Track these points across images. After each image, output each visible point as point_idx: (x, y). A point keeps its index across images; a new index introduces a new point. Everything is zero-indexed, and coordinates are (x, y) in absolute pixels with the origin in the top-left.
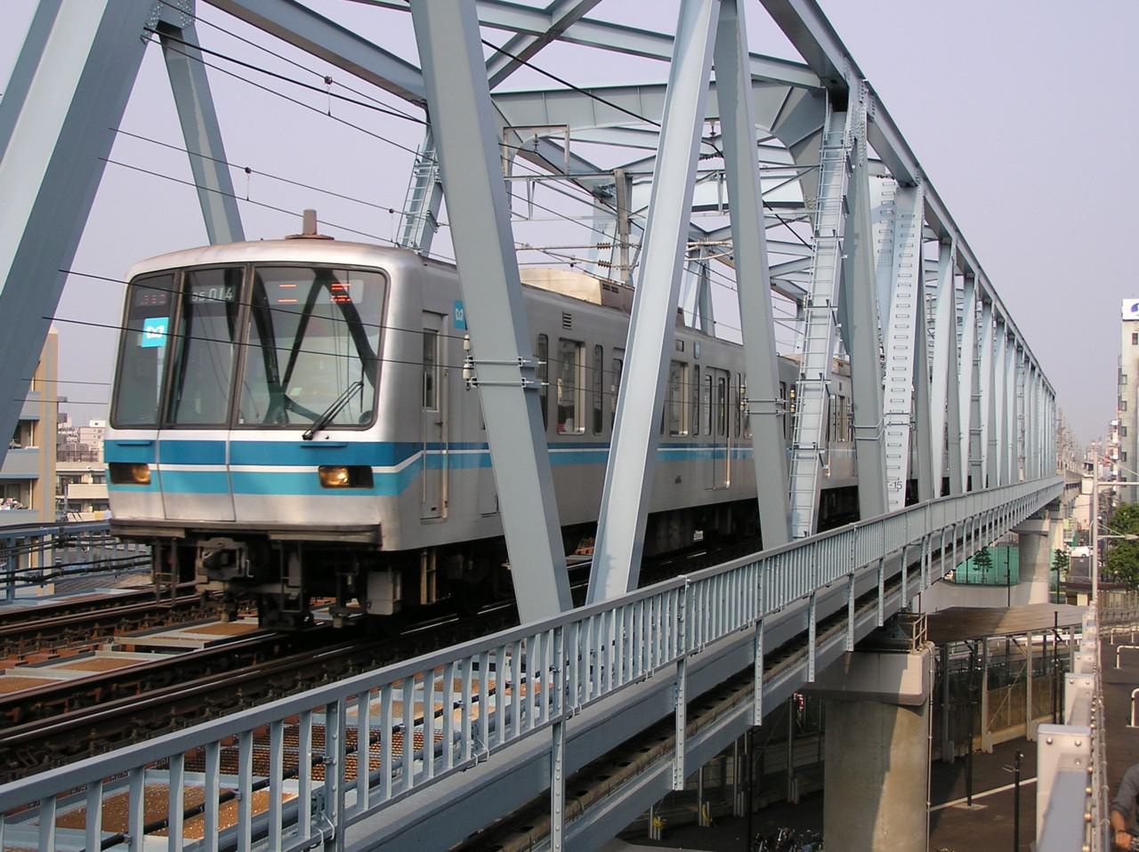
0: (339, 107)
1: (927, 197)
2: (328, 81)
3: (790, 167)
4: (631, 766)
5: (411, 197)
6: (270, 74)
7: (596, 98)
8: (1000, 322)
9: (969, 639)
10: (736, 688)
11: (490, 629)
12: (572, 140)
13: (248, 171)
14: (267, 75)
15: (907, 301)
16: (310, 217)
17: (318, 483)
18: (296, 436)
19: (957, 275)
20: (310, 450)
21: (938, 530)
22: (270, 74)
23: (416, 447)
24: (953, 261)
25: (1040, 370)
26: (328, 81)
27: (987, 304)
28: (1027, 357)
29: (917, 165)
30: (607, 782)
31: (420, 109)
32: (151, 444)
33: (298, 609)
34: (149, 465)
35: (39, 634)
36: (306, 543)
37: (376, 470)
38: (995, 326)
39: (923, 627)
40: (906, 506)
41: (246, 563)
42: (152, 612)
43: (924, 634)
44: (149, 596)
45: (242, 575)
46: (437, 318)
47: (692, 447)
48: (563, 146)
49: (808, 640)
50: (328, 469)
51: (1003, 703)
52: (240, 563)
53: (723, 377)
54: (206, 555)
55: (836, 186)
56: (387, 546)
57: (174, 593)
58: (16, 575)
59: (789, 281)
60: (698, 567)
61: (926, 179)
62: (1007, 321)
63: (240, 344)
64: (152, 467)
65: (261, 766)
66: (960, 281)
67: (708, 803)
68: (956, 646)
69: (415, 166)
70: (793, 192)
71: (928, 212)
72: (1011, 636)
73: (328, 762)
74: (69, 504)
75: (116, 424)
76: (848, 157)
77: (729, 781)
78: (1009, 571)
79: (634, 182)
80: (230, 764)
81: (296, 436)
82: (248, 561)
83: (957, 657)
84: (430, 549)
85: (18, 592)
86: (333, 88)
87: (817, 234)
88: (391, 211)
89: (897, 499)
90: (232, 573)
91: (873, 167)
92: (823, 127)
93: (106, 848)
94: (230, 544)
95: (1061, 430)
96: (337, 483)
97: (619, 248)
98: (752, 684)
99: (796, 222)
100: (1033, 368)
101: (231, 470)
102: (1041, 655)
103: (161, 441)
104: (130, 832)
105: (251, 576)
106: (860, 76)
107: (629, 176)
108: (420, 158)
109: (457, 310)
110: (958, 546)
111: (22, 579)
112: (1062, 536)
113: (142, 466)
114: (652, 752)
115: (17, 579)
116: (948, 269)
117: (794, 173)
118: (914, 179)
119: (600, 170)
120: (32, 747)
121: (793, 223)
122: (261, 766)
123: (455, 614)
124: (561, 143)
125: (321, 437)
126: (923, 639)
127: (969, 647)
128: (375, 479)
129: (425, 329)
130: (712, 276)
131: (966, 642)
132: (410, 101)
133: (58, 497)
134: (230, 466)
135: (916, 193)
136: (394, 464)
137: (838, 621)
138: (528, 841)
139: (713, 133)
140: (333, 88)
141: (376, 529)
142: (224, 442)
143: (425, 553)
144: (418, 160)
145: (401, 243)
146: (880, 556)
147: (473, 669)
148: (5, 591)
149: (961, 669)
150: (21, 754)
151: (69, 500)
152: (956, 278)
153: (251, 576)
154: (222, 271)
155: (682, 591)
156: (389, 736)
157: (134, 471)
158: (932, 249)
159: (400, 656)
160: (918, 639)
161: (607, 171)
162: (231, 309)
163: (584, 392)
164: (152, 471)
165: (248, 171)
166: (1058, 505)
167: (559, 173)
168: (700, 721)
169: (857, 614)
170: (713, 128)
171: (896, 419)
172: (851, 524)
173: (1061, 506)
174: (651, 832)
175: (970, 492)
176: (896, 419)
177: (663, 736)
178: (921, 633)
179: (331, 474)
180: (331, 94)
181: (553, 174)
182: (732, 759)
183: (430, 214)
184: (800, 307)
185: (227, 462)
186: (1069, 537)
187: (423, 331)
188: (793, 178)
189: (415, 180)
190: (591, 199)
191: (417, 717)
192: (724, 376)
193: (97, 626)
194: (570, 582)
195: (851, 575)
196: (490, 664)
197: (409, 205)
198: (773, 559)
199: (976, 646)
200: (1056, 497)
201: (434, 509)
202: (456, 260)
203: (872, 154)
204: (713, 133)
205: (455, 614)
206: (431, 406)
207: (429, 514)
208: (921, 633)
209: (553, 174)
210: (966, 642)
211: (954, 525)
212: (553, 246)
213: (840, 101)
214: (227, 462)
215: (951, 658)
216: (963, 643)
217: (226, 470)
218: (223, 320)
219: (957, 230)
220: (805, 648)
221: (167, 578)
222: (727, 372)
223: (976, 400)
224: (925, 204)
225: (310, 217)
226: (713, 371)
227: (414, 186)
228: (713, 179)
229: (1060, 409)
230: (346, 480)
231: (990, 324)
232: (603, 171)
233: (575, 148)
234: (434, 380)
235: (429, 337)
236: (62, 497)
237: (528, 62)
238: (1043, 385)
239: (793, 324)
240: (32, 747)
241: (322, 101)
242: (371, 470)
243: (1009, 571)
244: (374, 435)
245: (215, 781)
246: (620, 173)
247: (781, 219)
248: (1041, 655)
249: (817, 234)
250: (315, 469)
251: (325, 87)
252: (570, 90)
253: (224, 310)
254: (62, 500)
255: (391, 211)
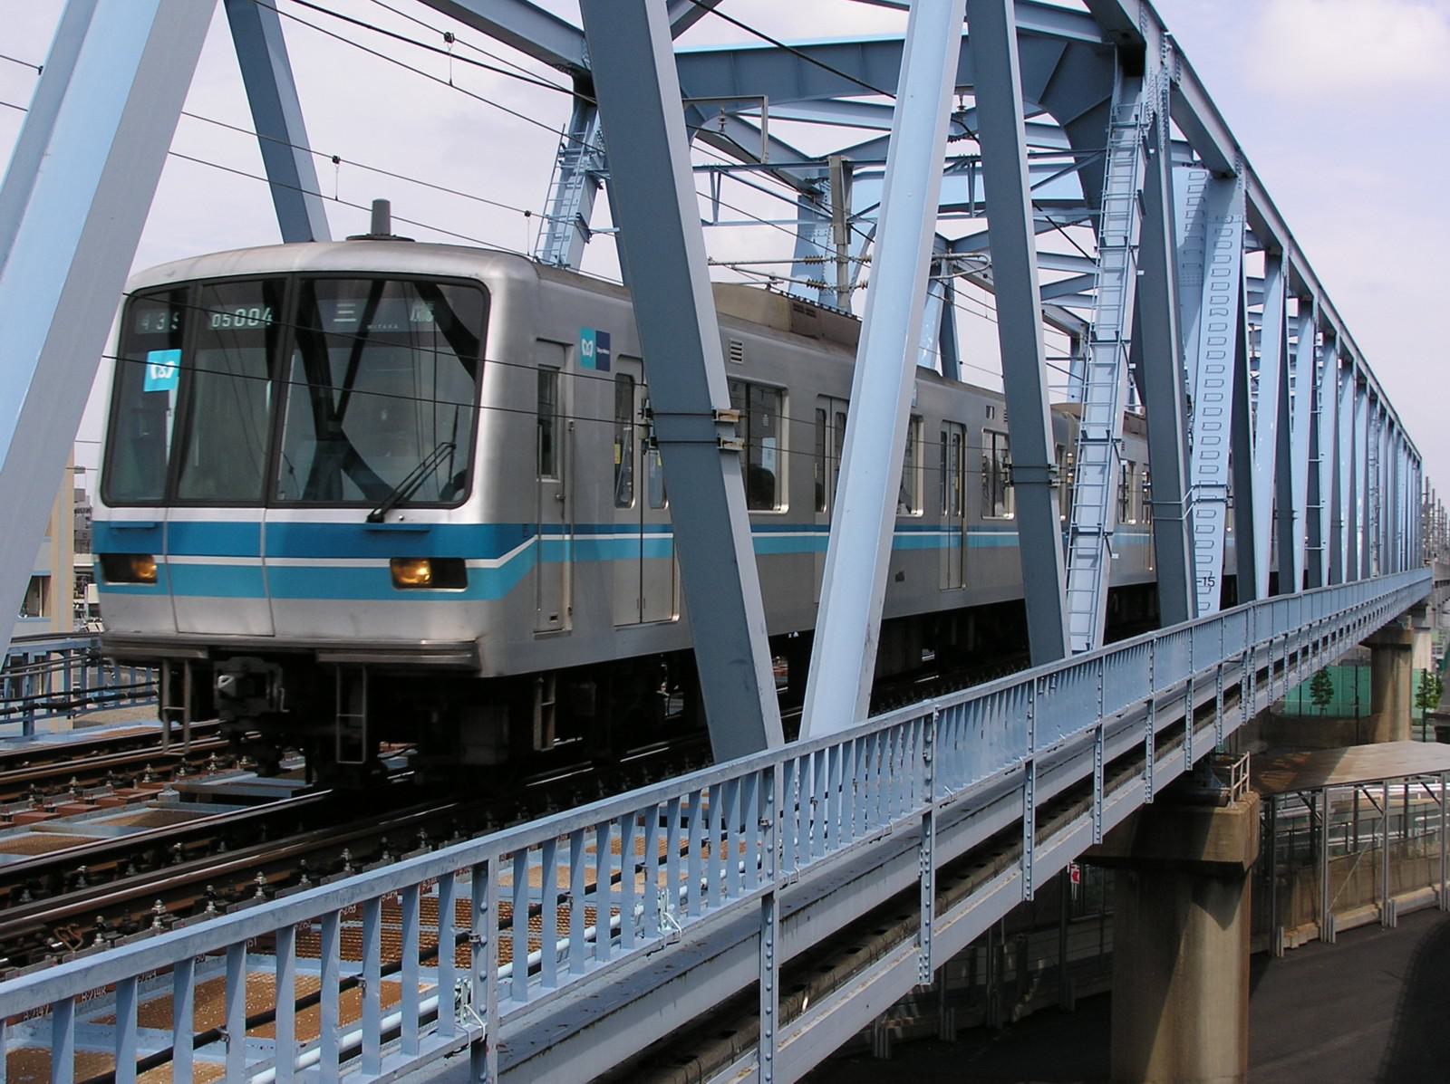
0: (463, 73)
1: (1249, 191)
2: (449, 38)
3: (1065, 153)
4: (862, 954)
5: (554, 195)
6: (369, 27)
7: (804, 57)
8: (1361, 385)
9: (1304, 790)
10: (885, 928)
11: (670, 773)
12: (770, 117)
13: (336, 160)
14: (366, 28)
15: (1213, 319)
16: (381, 210)
17: (389, 578)
18: (358, 516)
19: (1290, 297)
20: (374, 536)
21: (1264, 643)
22: (369, 27)
23: (525, 532)
24: (1285, 279)
25: (1401, 426)
26: (449, 38)
27: (1330, 338)
28: (1383, 409)
29: (1236, 148)
30: (831, 974)
31: (567, 75)
32: (156, 527)
33: (360, 760)
34: (155, 556)
35: (74, 778)
36: (371, 667)
37: (469, 564)
38: (1340, 366)
39: (1245, 771)
40: (1221, 609)
41: (280, 692)
42: (157, 761)
43: (1245, 781)
44: (150, 739)
45: (274, 710)
46: (557, 350)
47: (974, 531)
48: (759, 126)
49: (1093, 789)
50: (403, 562)
51: (1350, 875)
52: (272, 691)
53: (957, 433)
54: (224, 681)
55: (1123, 179)
56: (490, 669)
57: (187, 735)
58: (36, 701)
59: (1060, 307)
60: (952, 689)
61: (1249, 168)
62: (1356, 360)
63: (281, 382)
64: (159, 559)
65: (393, 945)
66: (1293, 306)
67: (953, 1010)
68: (1286, 799)
69: (559, 153)
70: (1070, 187)
71: (1252, 214)
72: (1361, 786)
73: (765, 824)
74: (90, 611)
75: (110, 501)
76: (1144, 137)
77: (981, 980)
78: (1357, 698)
79: (855, 173)
80: (353, 949)
81: (358, 516)
82: (283, 690)
83: (1287, 815)
84: (547, 674)
85: (39, 725)
86: (456, 48)
87: (1102, 243)
88: (528, 214)
89: (1209, 601)
90: (259, 706)
91: (1177, 156)
92: (1111, 97)
93: (144, 1071)
94: (259, 666)
95: (1427, 508)
96: (414, 581)
97: (835, 263)
98: (1020, 845)
99: (1071, 227)
100: (1391, 424)
101: (170, 562)
102: (1401, 811)
103: (170, 523)
104: (228, 1028)
105: (286, 711)
106: (1161, 28)
107: (849, 165)
108: (566, 141)
109: (584, 341)
110: (1275, 672)
111: (43, 706)
112: (1430, 652)
113: (146, 557)
114: (889, 935)
115: (37, 707)
116: (1309, 327)
117: (1071, 160)
118: (1233, 167)
119: (806, 158)
120: (74, 925)
121: (1067, 228)
122: (393, 945)
123: (590, 762)
124: (757, 122)
125: (397, 517)
126: (1244, 789)
127: (1305, 800)
128: (470, 577)
129: (540, 365)
130: (958, 299)
131: (1300, 794)
132: (552, 66)
133: (76, 601)
134: (267, 559)
135: (1233, 188)
136: (497, 554)
137: (1133, 764)
138: (730, 1051)
139: (962, 107)
140: (456, 48)
141: (472, 646)
142: (259, 524)
143: (541, 680)
144: (563, 145)
145: (540, 257)
146: (1188, 678)
147: (661, 825)
148: (21, 723)
149: (1294, 831)
150: (60, 932)
151: (90, 605)
152: (1288, 301)
153: (286, 711)
154: (261, 283)
155: (929, 720)
156: (521, 917)
157: (134, 565)
158: (1255, 264)
159: (553, 808)
160: (1238, 787)
161: (816, 159)
162: (270, 335)
163: (922, 470)
164: (157, 564)
165: (336, 160)
166: (1425, 610)
167: (752, 163)
168: (951, 895)
169: (1226, 707)
170: (961, 100)
171: (1206, 494)
172: (1150, 633)
173: (1429, 609)
174: (876, 1050)
175: (1307, 591)
176: (1206, 494)
177: (981, 863)
178: (1242, 779)
179: (405, 568)
180: (453, 56)
181: (744, 164)
182: (985, 949)
183: (581, 218)
184: (1075, 343)
185: (262, 554)
186: (1440, 653)
187: (537, 367)
188: (1066, 169)
189: (559, 172)
190: (794, 195)
191: (346, 975)
192: (956, 430)
193: (148, 769)
194: (781, 709)
195: (479, 1047)
196: (661, 817)
197: (551, 205)
198: (564, 850)
199: (1314, 799)
200: (1416, 600)
201: (553, 618)
202: (624, 283)
203: (1177, 134)
204: (962, 107)
205: (590, 762)
206: (549, 473)
207: (546, 625)
208: (1242, 779)
209: (744, 164)
210: (1300, 794)
211: (1310, 625)
212: (745, 261)
213: (1134, 65)
214: (165, 551)
215: (1278, 816)
216: (1297, 795)
217: (261, 564)
218: (261, 352)
219: (1290, 237)
220: (1090, 798)
221: (177, 716)
222: (963, 427)
223: (1314, 468)
224: (1247, 202)
225: (381, 210)
226: (828, 402)
227: (558, 181)
228: (960, 172)
229: (1427, 478)
230: (427, 577)
231: (1333, 363)
232: (812, 159)
233: (776, 129)
234: (553, 438)
235: (547, 377)
236: (81, 601)
237: (715, 8)
238: (1405, 447)
239: (1066, 365)
240: (74, 925)
241: (439, 65)
242: (463, 564)
243: (1357, 698)
244: (471, 513)
245: (304, 972)
246: (835, 164)
247: (1053, 223)
248: (1401, 811)
249: (1102, 243)
250: (385, 563)
251: (445, 46)
252: (775, 48)
253: (262, 338)
254: (81, 606)
255: (528, 214)
